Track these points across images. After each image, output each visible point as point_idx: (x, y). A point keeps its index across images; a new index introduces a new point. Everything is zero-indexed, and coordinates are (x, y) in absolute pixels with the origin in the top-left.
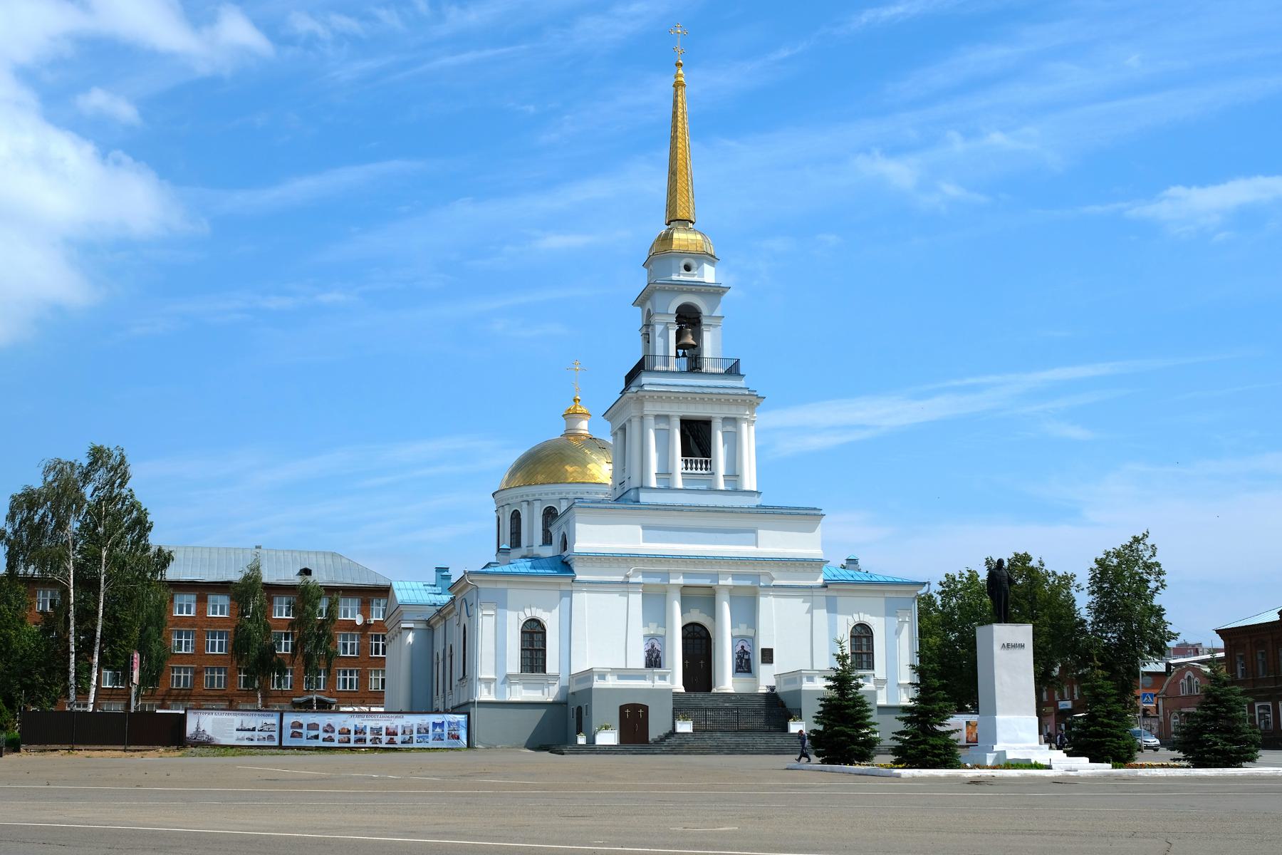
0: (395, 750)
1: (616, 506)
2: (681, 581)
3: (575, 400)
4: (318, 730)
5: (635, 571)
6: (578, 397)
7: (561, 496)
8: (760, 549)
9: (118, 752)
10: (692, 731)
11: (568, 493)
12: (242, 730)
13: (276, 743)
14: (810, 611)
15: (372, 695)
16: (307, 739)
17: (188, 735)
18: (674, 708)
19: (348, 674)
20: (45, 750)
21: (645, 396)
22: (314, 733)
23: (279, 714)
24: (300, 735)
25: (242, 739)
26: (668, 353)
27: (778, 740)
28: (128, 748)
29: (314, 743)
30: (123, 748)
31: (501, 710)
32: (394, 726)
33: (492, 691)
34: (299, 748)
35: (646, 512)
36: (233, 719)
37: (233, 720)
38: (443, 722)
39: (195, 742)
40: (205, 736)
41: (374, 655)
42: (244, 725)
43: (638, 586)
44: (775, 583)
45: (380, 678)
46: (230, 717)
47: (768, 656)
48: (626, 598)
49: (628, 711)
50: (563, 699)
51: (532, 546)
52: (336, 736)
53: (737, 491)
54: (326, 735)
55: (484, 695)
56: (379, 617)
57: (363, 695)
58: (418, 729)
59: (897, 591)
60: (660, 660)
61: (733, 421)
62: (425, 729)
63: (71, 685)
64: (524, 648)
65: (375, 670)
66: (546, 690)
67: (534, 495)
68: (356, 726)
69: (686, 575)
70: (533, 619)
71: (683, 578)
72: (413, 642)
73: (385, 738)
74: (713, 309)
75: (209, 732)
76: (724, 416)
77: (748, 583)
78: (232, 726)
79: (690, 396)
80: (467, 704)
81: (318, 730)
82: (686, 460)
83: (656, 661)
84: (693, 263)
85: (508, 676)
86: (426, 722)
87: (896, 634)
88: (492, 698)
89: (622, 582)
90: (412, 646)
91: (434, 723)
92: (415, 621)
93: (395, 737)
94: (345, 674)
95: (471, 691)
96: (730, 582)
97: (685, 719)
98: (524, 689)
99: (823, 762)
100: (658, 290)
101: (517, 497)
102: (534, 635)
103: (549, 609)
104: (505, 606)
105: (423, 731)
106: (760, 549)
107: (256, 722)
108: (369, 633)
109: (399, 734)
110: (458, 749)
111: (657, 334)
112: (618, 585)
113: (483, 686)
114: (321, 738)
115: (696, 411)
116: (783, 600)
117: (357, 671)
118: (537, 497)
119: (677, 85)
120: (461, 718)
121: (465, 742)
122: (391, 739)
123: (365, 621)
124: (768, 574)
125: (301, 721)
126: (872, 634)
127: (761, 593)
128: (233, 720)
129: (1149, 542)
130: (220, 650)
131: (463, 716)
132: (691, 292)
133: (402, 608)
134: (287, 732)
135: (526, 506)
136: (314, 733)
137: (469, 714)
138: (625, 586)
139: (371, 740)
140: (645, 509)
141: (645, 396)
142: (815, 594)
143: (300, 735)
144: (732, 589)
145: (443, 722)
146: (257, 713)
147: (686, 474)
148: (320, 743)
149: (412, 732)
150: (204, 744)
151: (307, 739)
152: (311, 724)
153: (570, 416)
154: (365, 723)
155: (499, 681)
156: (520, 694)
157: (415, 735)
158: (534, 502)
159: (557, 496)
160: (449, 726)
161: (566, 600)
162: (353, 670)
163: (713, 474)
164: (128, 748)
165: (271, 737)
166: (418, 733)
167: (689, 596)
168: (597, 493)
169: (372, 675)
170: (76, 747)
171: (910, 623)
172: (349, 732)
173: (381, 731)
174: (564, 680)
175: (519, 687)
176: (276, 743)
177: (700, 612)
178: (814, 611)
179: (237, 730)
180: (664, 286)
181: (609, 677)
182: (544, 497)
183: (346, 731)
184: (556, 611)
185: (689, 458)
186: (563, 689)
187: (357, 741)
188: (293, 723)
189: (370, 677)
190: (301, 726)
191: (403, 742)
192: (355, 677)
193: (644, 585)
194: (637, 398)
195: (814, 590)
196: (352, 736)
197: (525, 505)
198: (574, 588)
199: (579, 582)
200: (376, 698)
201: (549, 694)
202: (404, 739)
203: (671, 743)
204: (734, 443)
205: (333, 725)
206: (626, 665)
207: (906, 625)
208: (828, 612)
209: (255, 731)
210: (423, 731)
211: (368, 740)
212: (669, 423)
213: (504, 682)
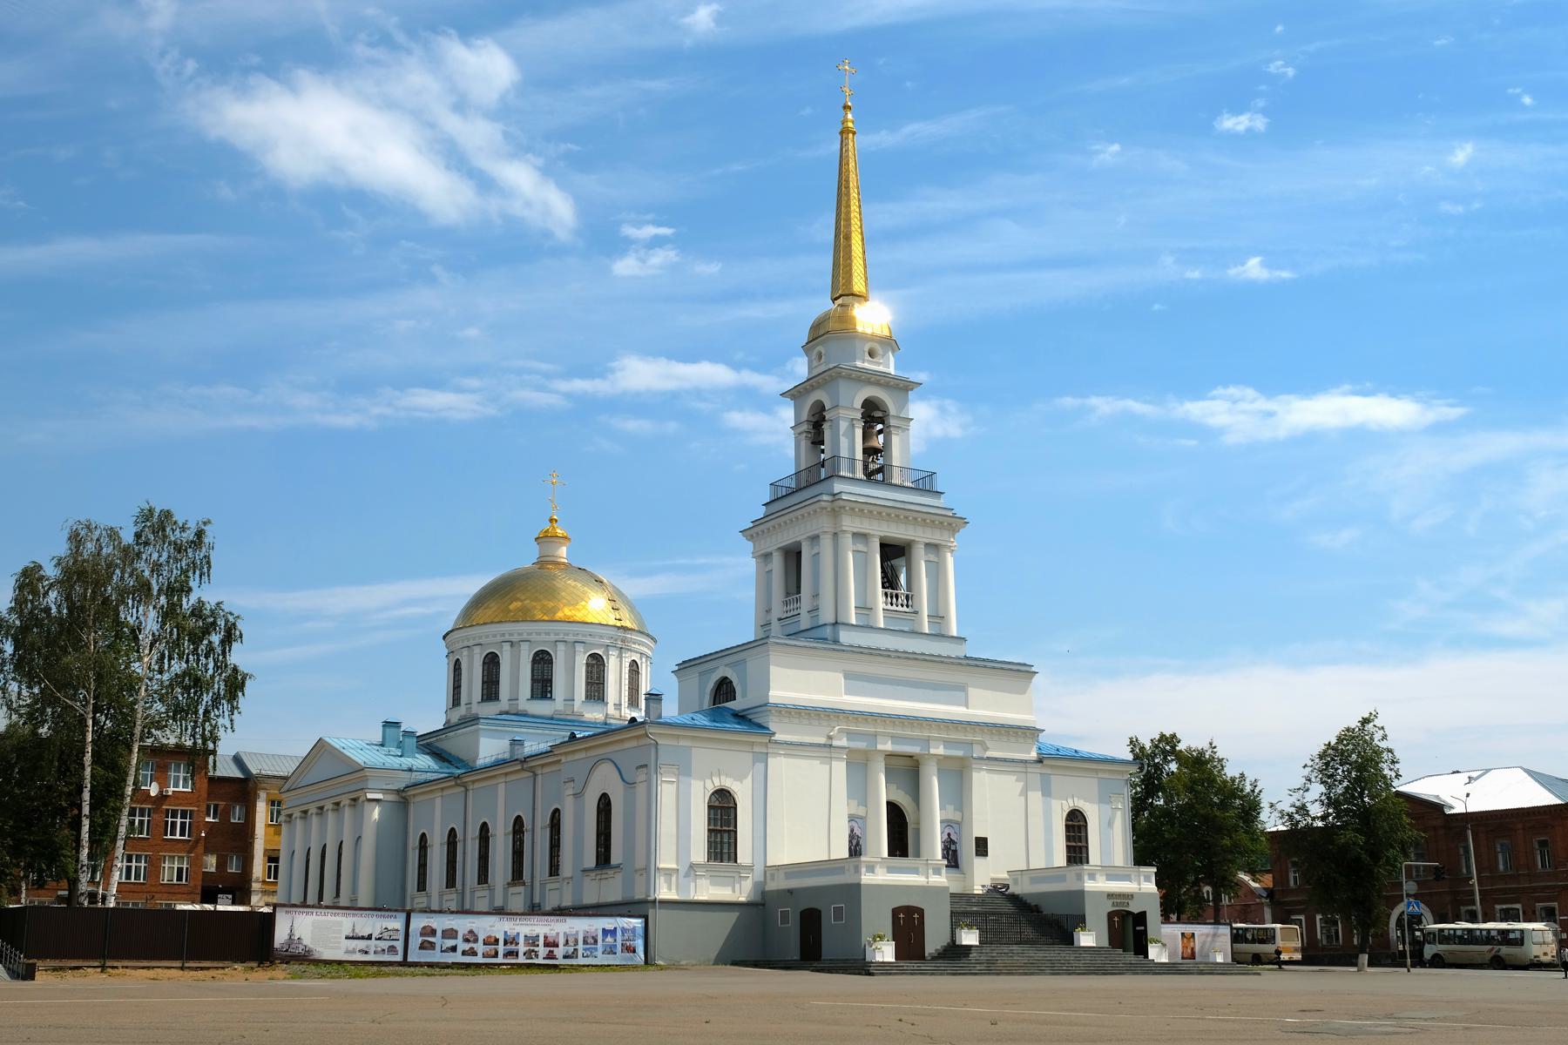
0: (555, 966)
1: (787, 642)
2: (887, 746)
3: (551, 520)
4: (456, 938)
5: (840, 731)
6: (555, 517)
7: (557, 638)
8: (971, 711)
10: (978, 944)
11: (480, 638)
12: (353, 938)
13: (399, 958)
16: (442, 951)
17: (277, 944)
18: (952, 912)
19: (134, 861)
20: (61, 969)
21: (844, 507)
22: (450, 943)
24: (432, 946)
25: (353, 952)
26: (854, 456)
27: (1056, 953)
28: (186, 965)
29: (451, 958)
30: (178, 964)
31: (684, 912)
32: (554, 933)
33: (674, 887)
34: (431, 965)
37: (340, 924)
38: (615, 928)
39: (286, 956)
40: (301, 947)
41: (169, 837)
43: (841, 751)
44: (990, 754)
45: (176, 866)
46: (338, 918)
47: (982, 846)
48: (828, 766)
49: (902, 916)
50: (758, 899)
51: (517, 699)
52: (480, 948)
53: (941, 636)
54: (467, 946)
55: (664, 892)
57: (153, 889)
58: (584, 938)
60: (860, 849)
61: (934, 547)
62: (593, 937)
63: (83, 866)
64: (711, 828)
65: (169, 856)
66: (737, 886)
67: (520, 634)
68: (506, 932)
71: (892, 743)
72: (379, 819)
73: (542, 951)
75: (307, 941)
77: (960, 753)
79: (884, 512)
80: (644, 902)
81: (456, 938)
85: (692, 866)
86: (594, 928)
88: (673, 896)
89: (825, 745)
90: (379, 824)
91: (604, 929)
93: (555, 949)
94: (129, 860)
95: (649, 885)
98: (711, 884)
100: (844, 377)
101: (495, 636)
102: (722, 809)
104: (688, 774)
105: (590, 940)
106: (971, 711)
107: (374, 927)
108: (164, 807)
109: (561, 945)
110: (635, 967)
111: (841, 433)
112: (818, 749)
113: (662, 879)
114: (459, 950)
115: (897, 532)
116: (996, 777)
117: (146, 856)
118: (525, 637)
120: (637, 923)
122: (551, 952)
123: (161, 792)
124: (982, 743)
125: (434, 926)
126: (1086, 822)
127: (974, 766)
129: (1377, 722)
130: (182, 834)
131: (639, 920)
132: (877, 384)
136: (450, 943)
137: (646, 918)
138: (827, 749)
139: (524, 954)
140: (847, 651)
141: (844, 507)
142: (1029, 770)
143: (432, 946)
144: (942, 760)
146: (375, 913)
147: (887, 610)
148: (458, 958)
150: (300, 959)
151: (442, 951)
153: (545, 539)
155: (682, 873)
157: (580, 946)
158: (521, 643)
159: (553, 638)
160: (623, 935)
162: (141, 856)
164: (186, 965)
165: (392, 949)
166: (584, 944)
168: (601, 637)
169: (165, 863)
170: (109, 963)
171: (1123, 810)
172: (497, 941)
173: (538, 941)
174: (758, 874)
176: (399, 958)
177: (897, 789)
178: (1029, 793)
179: (347, 938)
180: (851, 372)
181: (878, 869)
182: (533, 637)
183: (493, 940)
185: (889, 591)
186: (760, 888)
187: (507, 955)
188: (424, 928)
189: (163, 865)
190: (433, 932)
191: (565, 957)
192: (143, 865)
193: (850, 751)
194: (833, 510)
195: (1028, 765)
196: (501, 948)
197: (507, 647)
198: (770, 751)
199: (776, 742)
200: (169, 893)
201: (741, 892)
202: (567, 952)
205: (476, 932)
206: (829, 856)
207: (1119, 814)
208: (1043, 795)
210: (590, 940)
211: (521, 954)
213: (687, 875)
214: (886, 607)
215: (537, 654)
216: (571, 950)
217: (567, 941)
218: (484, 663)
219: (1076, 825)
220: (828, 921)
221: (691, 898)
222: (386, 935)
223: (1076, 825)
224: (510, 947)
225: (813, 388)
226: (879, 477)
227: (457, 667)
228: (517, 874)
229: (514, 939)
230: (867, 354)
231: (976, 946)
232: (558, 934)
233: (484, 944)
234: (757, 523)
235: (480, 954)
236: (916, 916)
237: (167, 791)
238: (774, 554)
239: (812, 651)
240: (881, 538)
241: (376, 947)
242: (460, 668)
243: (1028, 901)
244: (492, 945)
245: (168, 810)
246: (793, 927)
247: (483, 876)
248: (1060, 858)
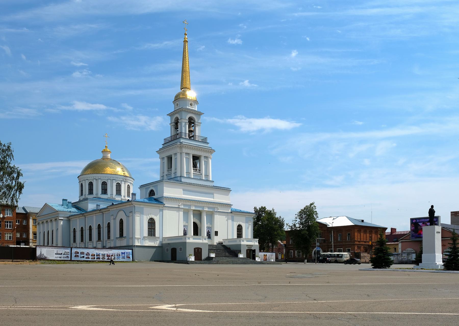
2: (194, 208)
3: (106, 147)
4: (84, 254)
6: (107, 146)
9: (10, 262)
11: (101, 177)
12: (57, 254)
13: (69, 259)
14: (227, 220)
15: (6, 241)
17: (37, 256)
22: (82, 255)
23: (70, 249)
24: (78, 256)
27: (234, 259)
28: (13, 261)
29: (83, 259)
30: (11, 260)
34: (78, 261)
35: (184, 185)
36: (54, 250)
37: (54, 250)
40: (44, 256)
42: (58, 252)
44: (219, 211)
45: (9, 236)
47: (216, 233)
48: (178, 213)
50: (161, 245)
51: (98, 194)
52: (90, 257)
54: (87, 256)
55: (137, 244)
56: (8, 215)
59: (248, 215)
65: (7, 233)
66: (155, 242)
67: (98, 177)
68: (97, 253)
69: (195, 206)
70: (152, 218)
73: (106, 258)
74: (199, 119)
75: (45, 255)
76: (205, 156)
77: (212, 210)
78: (54, 252)
80: (132, 246)
81: (84, 254)
82: (194, 169)
83: (185, 234)
84: (193, 103)
85: (144, 237)
87: (248, 228)
88: (139, 244)
90: (62, 225)
92: (63, 217)
96: (207, 209)
97: (213, 253)
99: (373, 268)
100: (183, 111)
101: (91, 177)
102: (152, 223)
103: (156, 215)
104: (143, 214)
105: (118, 255)
107: (62, 251)
110: (130, 262)
113: (136, 240)
115: (197, 153)
116: (220, 216)
118: (100, 178)
119: (185, 42)
120: (130, 251)
121: (132, 259)
122: (108, 258)
123: (3, 216)
124: (217, 208)
125: (78, 251)
128: (54, 250)
130: (10, 227)
131: (131, 250)
132: (192, 113)
133: (59, 212)
134: (73, 255)
135: (95, 181)
136: (82, 255)
137: (132, 250)
139: (102, 258)
141: (183, 146)
143: (78, 256)
146: (63, 248)
148: (85, 259)
149: (115, 255)
150: (44, 259)
152: (82, 252)
154: (100, 252)
155: (141, 239)
156: (148, 243)
157: (116, 257)
159: (107, 178)
161: (161, 212)
163: (201, 174)
164: (13, 261)
165: (68, 257)
167: (198, 214)
171: (251, 226)
172: (94, 255)
175: (147, 241)
176: (69, 259)
177: (196, 219)
181: (191, 239)
182: (102, 178)
183: (93, 255)
184: (158, 216)
187: (97, 258)
188: (76, 252)
190: (78, 253)
196: (96, 257)
197: (95, 180)
200: (8, 242)
201: (157, 244)
203: (209, 259)
204: (207, 164)
207: (250, 226)
208: (232, 221)
209: (62, 254)
210: (118, 255)
211: (101, 258)
212: (189, 156)
213: (143, 239)
214: (194, 173)
219: (240, 228)
222: (66, 253)
225: (176, 113)
226: (193, 138)
229: (99, 255)
234: (160, 149)
239: (168, 182)
240: (193, 154)
245: (5, 221)
246: (170, 252)
247: (90, 239)
248: (235, 236)
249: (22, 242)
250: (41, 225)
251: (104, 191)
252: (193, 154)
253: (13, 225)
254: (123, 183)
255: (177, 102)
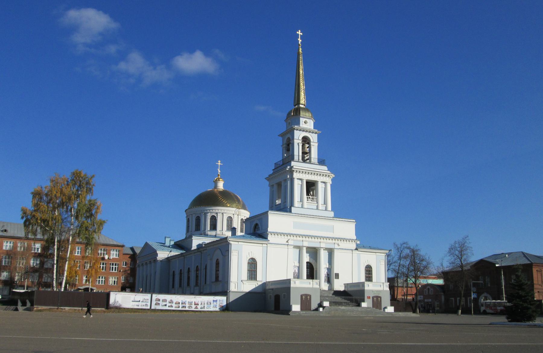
12: (134, 301)
13: (149, 308)
22: (165, 303)
24: (159, 304)
25: (134, 305)
38: (217, 300)
47: (337, 276)
50: (260, 290)
52: (174, 305)
54: (170, 304)
56: (503, 300)
62: (210, 303)
68: (182, 301)
91: (213, 300)
93: (198, 306)
99: (509, 321)
102: (253, 264)
122: (196, 307)
123: (109, 258)
130: (115, 270)
132: (307, 131)
136: (165, 303)
139: (188, 307)
143: (159, 304)
145: (217, 300)
149: (204, 304)
151: (162, 306)
152: (164, 300)
157: (206, 305)
160: (219, 302)
165: (146, 305)
172: (179, 303)
176: (149, 308)
179: (133, 301)
183: (178, 303)
190: (159, 300)
191: (201, 308)
196: (181, 305)
197: (191, 216)
210: (209, 303)
211: (187, 307)
215: (197, 217)
216: (203, 306)
217: (202, 304)
218: (196, 219)
219: (369, 270)
220: (282, 298)
221: (242, 291)
222: (144, 301)
223: (369, 270)
224: (183, 305)
225: (287, 133)
226: (308, 161)
227: (188, 221)
228: (197, 285)
229: (185, 303)
230: (304, 122)
231: (328, 307)
232: (199, 301)
233: (175, 304)
234: (270, 175)
235: (174, 307)
236: (308, 297)
237: (110, 258)
238: (275, 185)
239: (284, 216)
240: (306, 180)
241: (141, 304)
242: (189, 221)
243: (349, 293)
244: (178, 304)
245: (85, 262)
246: (273, 299)
247: (188, 284)
248: (363, 279)
249: (128, 288)
250: (145, 266)
251: (214, 227)
252: (306, 180)
253: (119, 268)
254: (236, 216)
255: (289, 121)
